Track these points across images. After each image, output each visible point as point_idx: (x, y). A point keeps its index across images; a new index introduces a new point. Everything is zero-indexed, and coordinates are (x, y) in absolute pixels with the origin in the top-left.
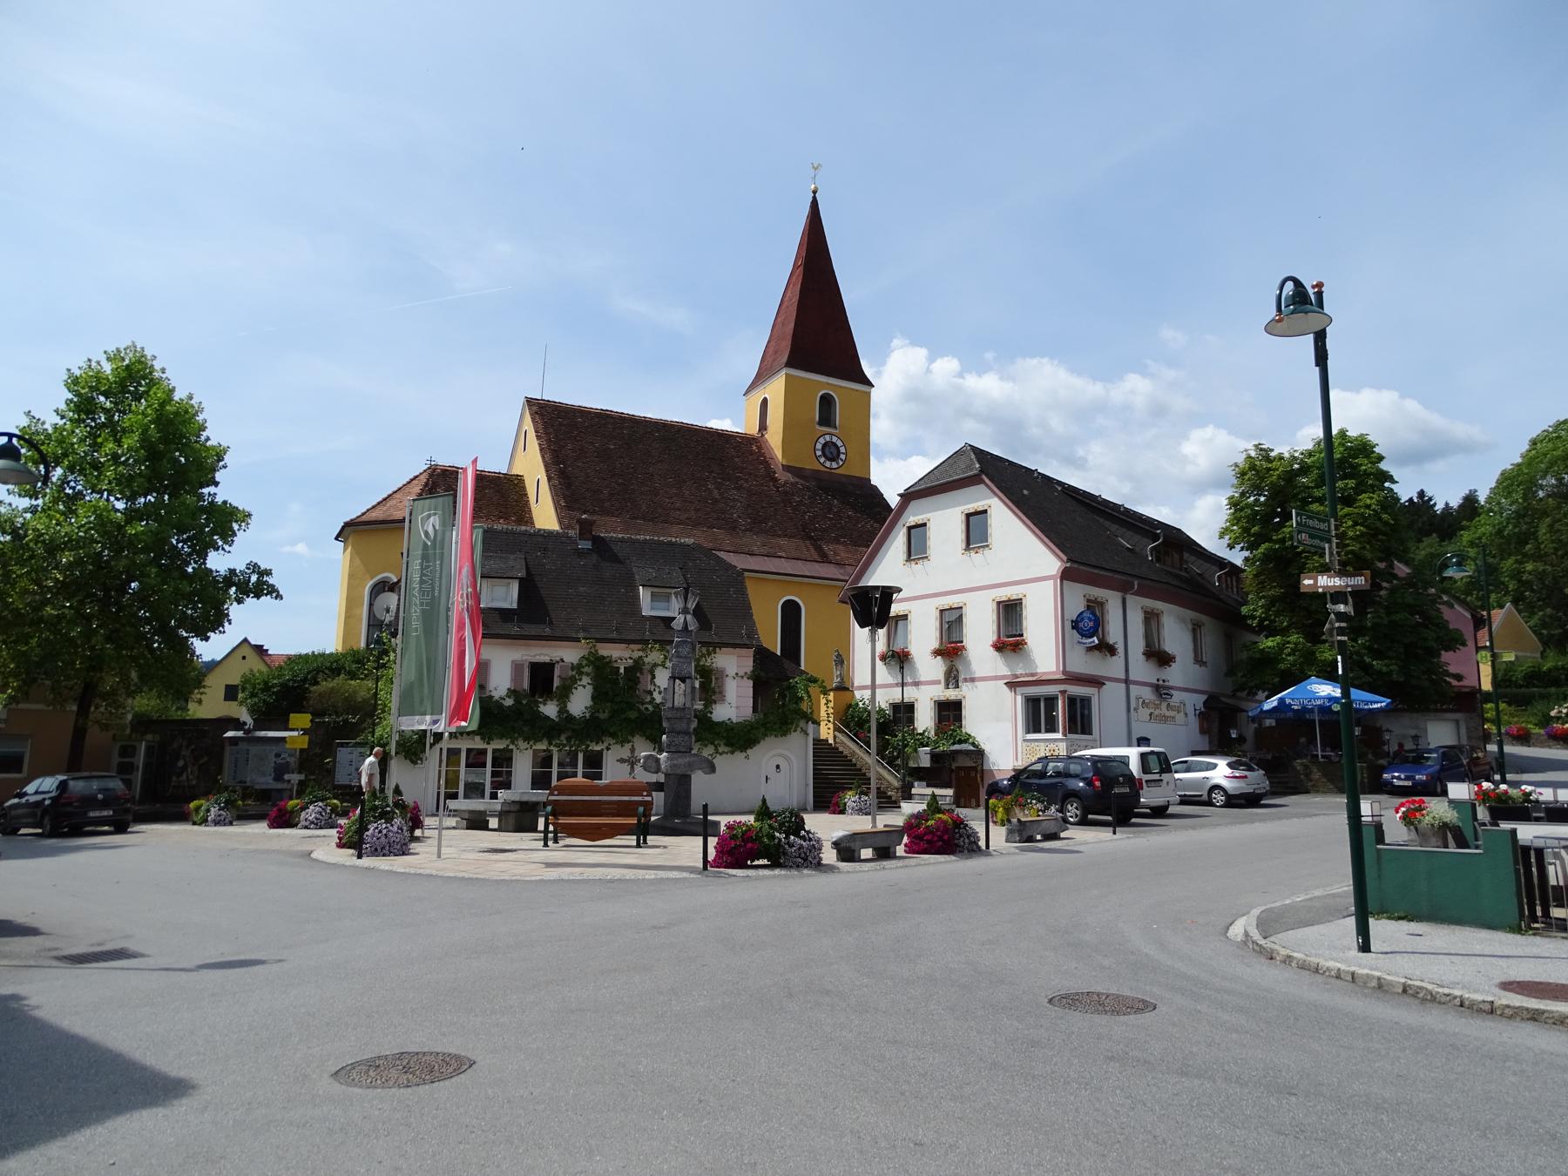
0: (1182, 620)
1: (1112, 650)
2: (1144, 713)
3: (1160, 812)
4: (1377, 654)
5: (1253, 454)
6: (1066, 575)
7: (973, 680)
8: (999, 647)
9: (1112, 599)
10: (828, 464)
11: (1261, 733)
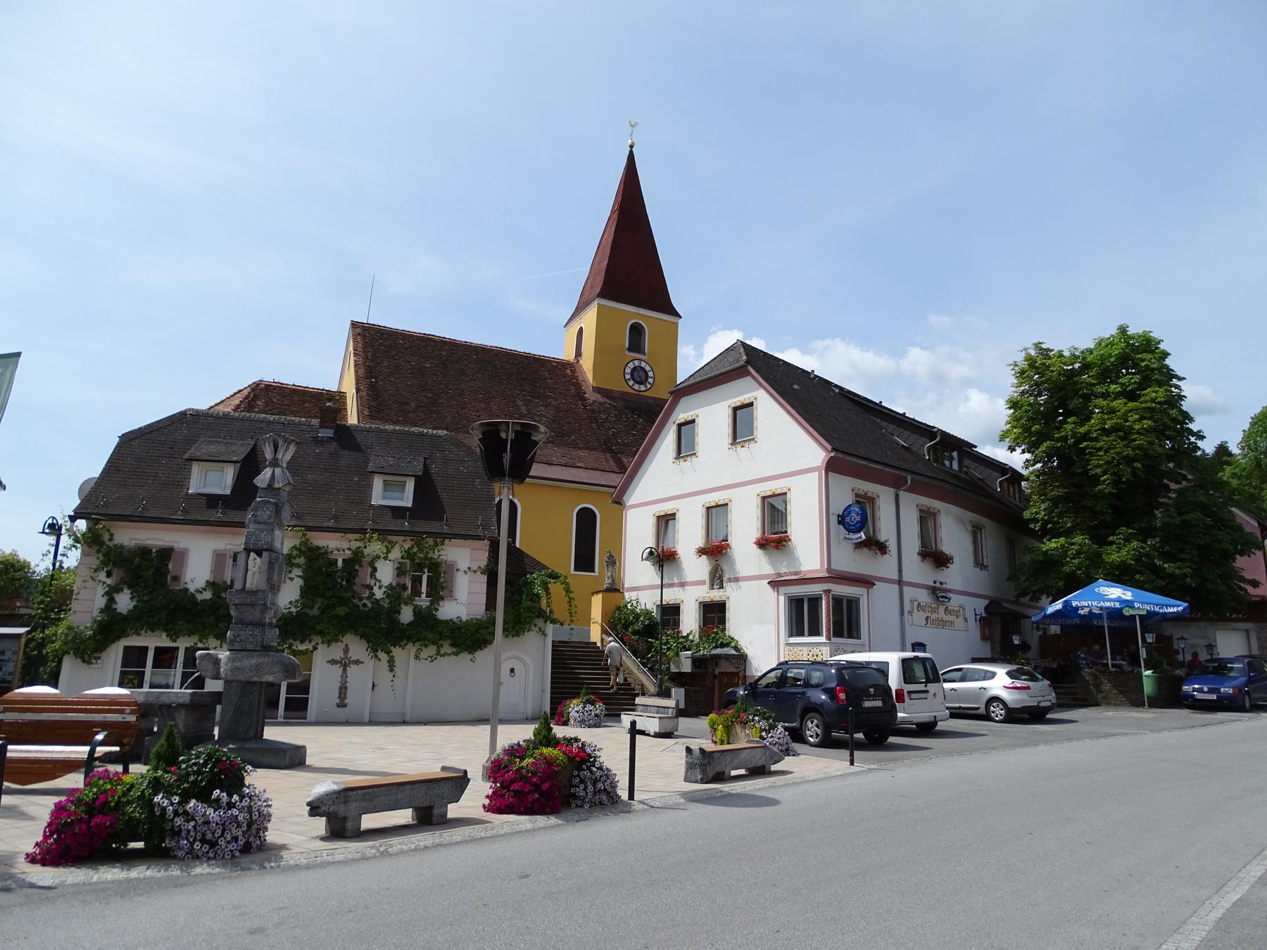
0: (961, 521)
1: (882, 548)
2: (919, 617)
3: (927, 729)
4: (1169, 557)
5: (1033, 353)
6: (832, 466)
7: (737, 580)
8: (762, 544)
9: (884, 496)
10: (636, 387)
11: (1046, 640)
